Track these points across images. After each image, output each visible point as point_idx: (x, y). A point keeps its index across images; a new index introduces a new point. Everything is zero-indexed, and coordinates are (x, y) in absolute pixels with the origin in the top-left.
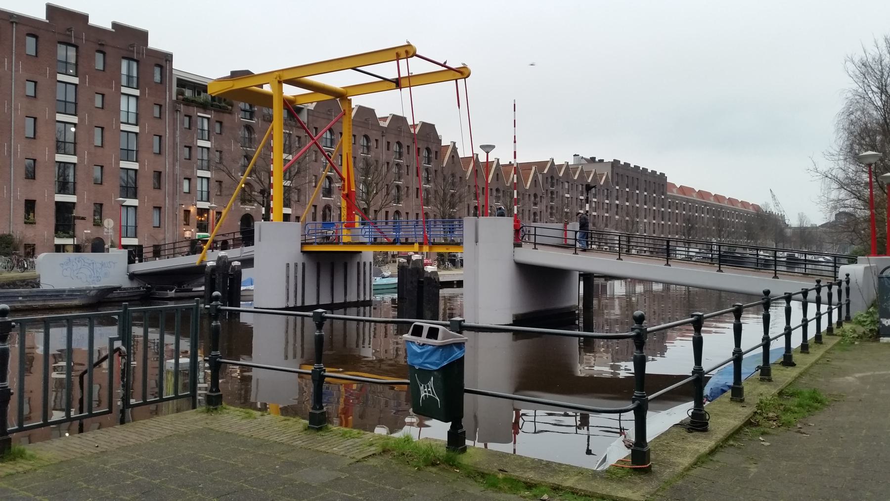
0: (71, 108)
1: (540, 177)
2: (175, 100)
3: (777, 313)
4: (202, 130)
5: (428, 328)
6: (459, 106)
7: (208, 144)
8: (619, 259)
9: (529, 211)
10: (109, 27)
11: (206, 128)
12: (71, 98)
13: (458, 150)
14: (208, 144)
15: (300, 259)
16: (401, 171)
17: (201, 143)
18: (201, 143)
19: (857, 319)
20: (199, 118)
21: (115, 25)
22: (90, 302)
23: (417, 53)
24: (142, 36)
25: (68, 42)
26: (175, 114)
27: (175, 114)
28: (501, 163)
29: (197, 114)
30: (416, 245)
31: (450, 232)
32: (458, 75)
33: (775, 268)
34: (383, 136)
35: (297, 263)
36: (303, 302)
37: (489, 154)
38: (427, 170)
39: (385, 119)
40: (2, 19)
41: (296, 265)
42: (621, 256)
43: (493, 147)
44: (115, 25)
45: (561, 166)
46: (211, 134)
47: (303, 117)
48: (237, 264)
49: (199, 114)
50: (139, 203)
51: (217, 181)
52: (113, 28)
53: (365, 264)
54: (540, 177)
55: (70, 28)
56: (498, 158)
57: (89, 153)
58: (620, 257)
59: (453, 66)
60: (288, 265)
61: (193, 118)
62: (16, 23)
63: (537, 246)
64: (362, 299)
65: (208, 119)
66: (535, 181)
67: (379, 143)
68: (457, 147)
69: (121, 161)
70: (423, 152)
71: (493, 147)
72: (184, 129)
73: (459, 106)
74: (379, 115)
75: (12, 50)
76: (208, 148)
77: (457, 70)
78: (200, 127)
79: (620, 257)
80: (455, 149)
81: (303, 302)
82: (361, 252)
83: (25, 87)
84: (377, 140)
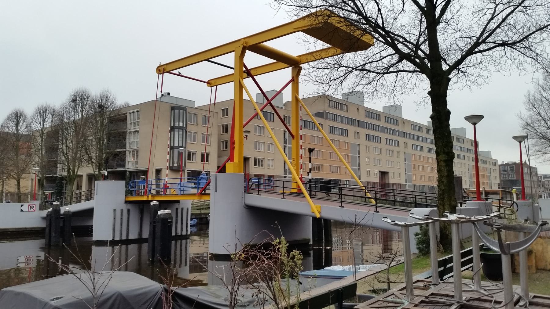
3: (512, 175)
5: (333, 263)
8: (283, 198)
15: (125, 207)
19: (18, 141)
22: (149, 223)
31: (269, 180)
33: (416, 200)
36: (128, 235)
37: (476, 126)
40: (549, 178)
42: (342, 204)
43: (481, 117)
45: (544, 76)
53: (182, 209)
58: (283, 197)
60: (115, 210)
71: (481, 117)
79: (283, 197)
81: (128, 235)
82: (178, 201)
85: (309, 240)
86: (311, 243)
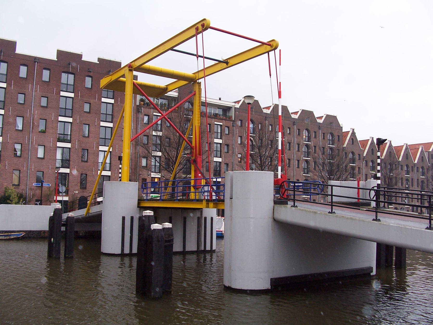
0: (109, 118)
1: (426, 154)
2: (138, 105)
4: (217, 133)
6: (270, 75)
7: (220, 141)
9: (418, 179)
10: (96, 61)
11: (219, 131)
12: (69, 106)
13: (356, 134)
14: (220, 141)
16: (309, 150)
17: (216, 141)
18: (216, 141)
20: (215, 125)
21: (60, 53)
23: (211, 25)
24: (80, 56)
25: (68, 71)
26: (138, 113)
27: (138, 113)
28: (394, 145)
29: (214, 123)
30: (204, 202)
32: (269, 48)
34: (294, 125)
35: (124, 217)
38: (307, 146)
39: (321, 118)
41: (132, 218)
44: (60, 53)
46: (163, 127)
47: (232, 113)
48: (148, 214)
49: (215, 123)
50: (119, 175)
51: (225, 164)
52: (98, 61)
53: (205, 218)
54: (426, 154)
55: (109, 71)
56: (373, 137)
57: (79, 141)
59: (265, 41)
60: (124, 218)
61: (150, 117)
62: (37, 62)
63: (335, 209)
64: (203, 248)
65: (221, 125)
66: (422, 158)
67: (292, 130)
68: (355, 132)
69: (100, 146)
70: (327, 136)
72: (143, 124)
73: (270, 75)
74: (316, 116)
75: (34, 78)
76: (220, 144)
77: (268, 44)
78: (216, 131)
80: (353, 133)
83: (40, 101)
84: (315, 132)
85: (371, 269)
86: (374, 273)
